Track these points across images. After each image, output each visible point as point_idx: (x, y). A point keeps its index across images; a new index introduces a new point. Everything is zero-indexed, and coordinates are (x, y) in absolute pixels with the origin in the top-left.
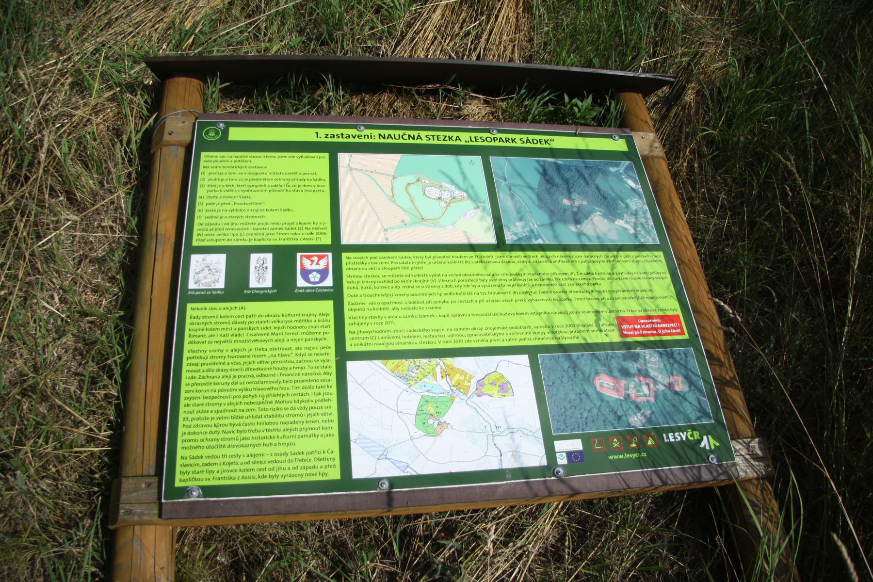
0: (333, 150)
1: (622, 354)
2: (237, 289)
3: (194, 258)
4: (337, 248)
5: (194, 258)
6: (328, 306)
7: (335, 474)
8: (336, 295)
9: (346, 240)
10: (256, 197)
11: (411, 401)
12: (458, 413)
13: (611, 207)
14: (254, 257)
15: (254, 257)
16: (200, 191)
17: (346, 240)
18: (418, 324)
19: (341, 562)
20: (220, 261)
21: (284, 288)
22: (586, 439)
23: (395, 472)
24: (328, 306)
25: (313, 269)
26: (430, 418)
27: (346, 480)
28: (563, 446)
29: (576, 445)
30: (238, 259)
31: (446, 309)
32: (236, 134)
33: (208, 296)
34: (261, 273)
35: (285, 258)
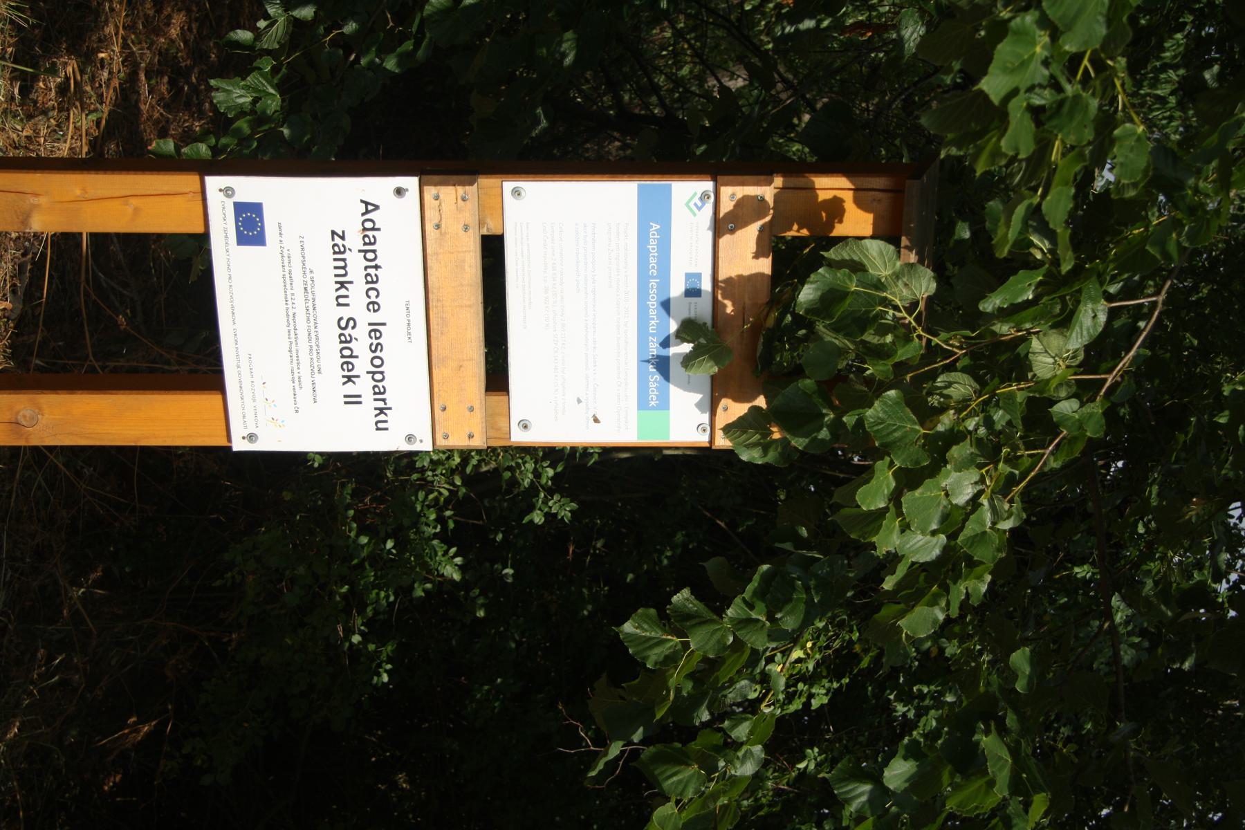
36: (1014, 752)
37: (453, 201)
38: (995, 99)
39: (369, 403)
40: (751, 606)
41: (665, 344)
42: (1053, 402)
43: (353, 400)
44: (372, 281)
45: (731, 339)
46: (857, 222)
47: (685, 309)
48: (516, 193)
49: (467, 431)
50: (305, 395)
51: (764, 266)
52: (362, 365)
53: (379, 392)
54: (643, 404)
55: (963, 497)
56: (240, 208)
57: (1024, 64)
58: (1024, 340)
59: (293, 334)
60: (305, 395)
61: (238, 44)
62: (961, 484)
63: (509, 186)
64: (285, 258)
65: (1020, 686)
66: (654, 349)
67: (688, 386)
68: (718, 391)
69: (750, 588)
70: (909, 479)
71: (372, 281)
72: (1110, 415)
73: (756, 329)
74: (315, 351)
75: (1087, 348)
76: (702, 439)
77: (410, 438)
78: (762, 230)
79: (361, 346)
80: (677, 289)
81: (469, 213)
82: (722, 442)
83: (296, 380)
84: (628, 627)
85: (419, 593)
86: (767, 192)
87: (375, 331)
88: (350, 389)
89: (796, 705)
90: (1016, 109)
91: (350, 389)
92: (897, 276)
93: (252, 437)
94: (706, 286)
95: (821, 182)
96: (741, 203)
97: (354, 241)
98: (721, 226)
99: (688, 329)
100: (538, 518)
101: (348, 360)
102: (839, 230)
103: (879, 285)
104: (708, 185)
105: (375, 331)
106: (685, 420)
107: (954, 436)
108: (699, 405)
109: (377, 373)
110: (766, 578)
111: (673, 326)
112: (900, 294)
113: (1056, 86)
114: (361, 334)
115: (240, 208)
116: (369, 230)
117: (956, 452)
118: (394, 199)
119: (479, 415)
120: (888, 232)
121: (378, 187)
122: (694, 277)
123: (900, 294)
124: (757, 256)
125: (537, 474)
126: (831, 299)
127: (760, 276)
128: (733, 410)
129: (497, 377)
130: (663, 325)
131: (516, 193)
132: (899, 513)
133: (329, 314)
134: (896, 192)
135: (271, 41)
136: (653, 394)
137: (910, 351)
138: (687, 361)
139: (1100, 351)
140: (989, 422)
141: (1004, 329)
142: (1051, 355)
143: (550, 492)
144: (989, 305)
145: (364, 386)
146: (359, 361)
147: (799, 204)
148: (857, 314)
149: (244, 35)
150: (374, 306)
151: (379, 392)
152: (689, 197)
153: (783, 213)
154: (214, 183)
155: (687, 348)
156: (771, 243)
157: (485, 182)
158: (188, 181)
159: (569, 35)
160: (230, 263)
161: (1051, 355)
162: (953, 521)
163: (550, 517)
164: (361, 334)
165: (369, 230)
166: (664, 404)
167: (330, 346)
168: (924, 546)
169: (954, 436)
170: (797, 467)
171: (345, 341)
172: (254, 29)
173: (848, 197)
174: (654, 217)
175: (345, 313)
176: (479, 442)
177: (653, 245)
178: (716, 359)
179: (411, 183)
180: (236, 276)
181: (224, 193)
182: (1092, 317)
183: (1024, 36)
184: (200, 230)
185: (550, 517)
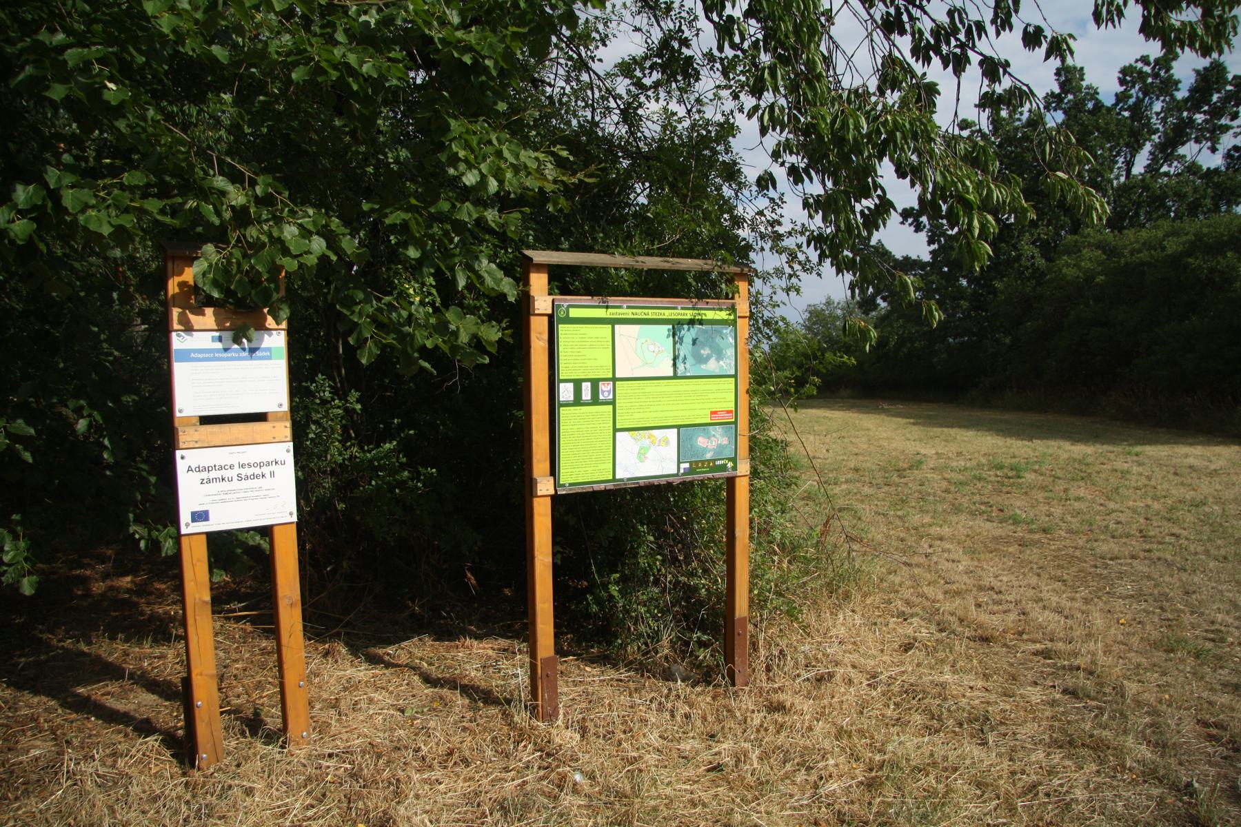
0: (613, 322)
1: (716, 421)
2: (577, 401)
3: (562, 385)
4: (614, 379)
5: (562, 385)
6: (611, 407)
7: (611, 477)
8: (613, 403)
9: (610, 376)
10: (583, 352)
11: (636, 448)
12: (651, 453)
13: (720, 355)
14: (584, 384)
15: (584, 384)
16: (561, 349)
17: (610, 376)
18: (642, 415)
19: (1207, 27)
20: (571, 385)
21: (595, 401)
22: (691, 463)
23: (629, 476)
24: (611, 407)
25: (605, 390)
26: (642, 456)
27: (614, 479)
28: (683, 466)
29: (687, 465)
30: (578, 384)
31: (652, 408)
32: (574, 313)
33: (567, 405)
34: (586, 395)
35: (595, 383)
36: (398, 209)
37: (185, 436)
38: (112, 230)
39: (273, 468)
40: (353, 312)
41: (244, 349)
42: (257, 196)
43: (272, 474)
44: (221, 468)
45: (239, 323)
46: (189, 275)
47: (229, 343)
48: (180, 411)
49: (284, 429)
50: (271, 493)
51: (209, 311)
52: (257, 471)
53: (268, 464)
54: (269, 358)
55: (294, 230)
56: (194, 520)
57: (99, 219)
58: (232, 207)
59: (245, 498)
60: (271, 493)
61: (147, 546)
62: (290, 232)
63: (178, 414)
64: (214, 502)
65: (377, 207)
66: (246, 354)
67: (262, 340)
68: (261, 327)
69: (345, 311)
70: (286, 252)
71: (221, 468)
72: (264, 171)
73: (235, 313)
74: (252, 489)
75: (233, 183)
76: (283, 334)
77: (288, 451)
78: (193, 313)
79: (249, 471)
80: (219, 345)
81: (191, 430)
82: (284, 325)
83: (265, 497)
84: (364, 361)
85: (404, 460)
86: (176, 312)
87: (242, 466)
88: (268, 475)
89: (434, 291)
90: (115, 222)
91: (268, 475)
92: (207, 259)
93: (291, 514)
94: (217, 334)
95: (171, 293)
96: (180, 323)
97: (205, 475)
98: (189, 328)
99: (237, 340)
100: (358, 407)
101: (255, 476)
102: (192, 283)
103: (210, 266)
104: (174, 334)
105: (242, 466)
106: (276, 340)
107: (270, 236)
108: (270, 335)
109: (260, 465)
110: (343, 306)
111: (236, 346)
112: (215, 258)
113: (108, 207)
114: (244, 472)
115: (194, 520)
116: (199, 469)
117: (275, 234)
118: (185, 461)
119: (276, 424)
120: (190, 261)
121: (181, 466)
122: (213, 339)
123: (215, 258)
124: (204, 314)
125: (339, 407)
126: (216, 284)
127: (215, 314)
128: (270, 322)
129: (261, 417)
130: (235, 351)
131: (180, 411)
132: (301, 255)
133: (236, 484)
134: (174, 258)
135: (145, 532)
136: (265, 354)
137: (237, 253)
138: (249, 341)
139: (235, 178)
140: (267, 221)
141: (227, 215)
142: (237, 197)
143: (347, 401)
144: (217, 221)
145: (266, 470)
146: (256, 472)
147: (176, 300)
148: (222, 276)
149: (142, 544)
150: (231, 467)
151: (268, 464)
152: (178, 342)
153: (185, 306)
154: (184, 531)
155: (244, 340)
156: (199, 312)
157: (177, 424)
158: (184, 541)
159: (124, 399)
160: (217, 523)
161: (237, 197)
162: (305, 233)
163: (358, 401)
164: (244, 472)
165: (199, 469)
166: (269, 349)
167: (245, 484)
168: (318, 244)
169: (270, 236)
170: (291, 297)
171: (247, 478)
172: (139, 540)
173: (177, 279)
174: (187, 356)
175: (235, 478)
176: (288, 424)
177: (200, 356)
178: (248, 329)
179: (178, 453)
180: (221, 521)
181: (187, 526)
182: (220, 182)
183: (87, 220)
184: (204, 537)
185: (358, 401)
